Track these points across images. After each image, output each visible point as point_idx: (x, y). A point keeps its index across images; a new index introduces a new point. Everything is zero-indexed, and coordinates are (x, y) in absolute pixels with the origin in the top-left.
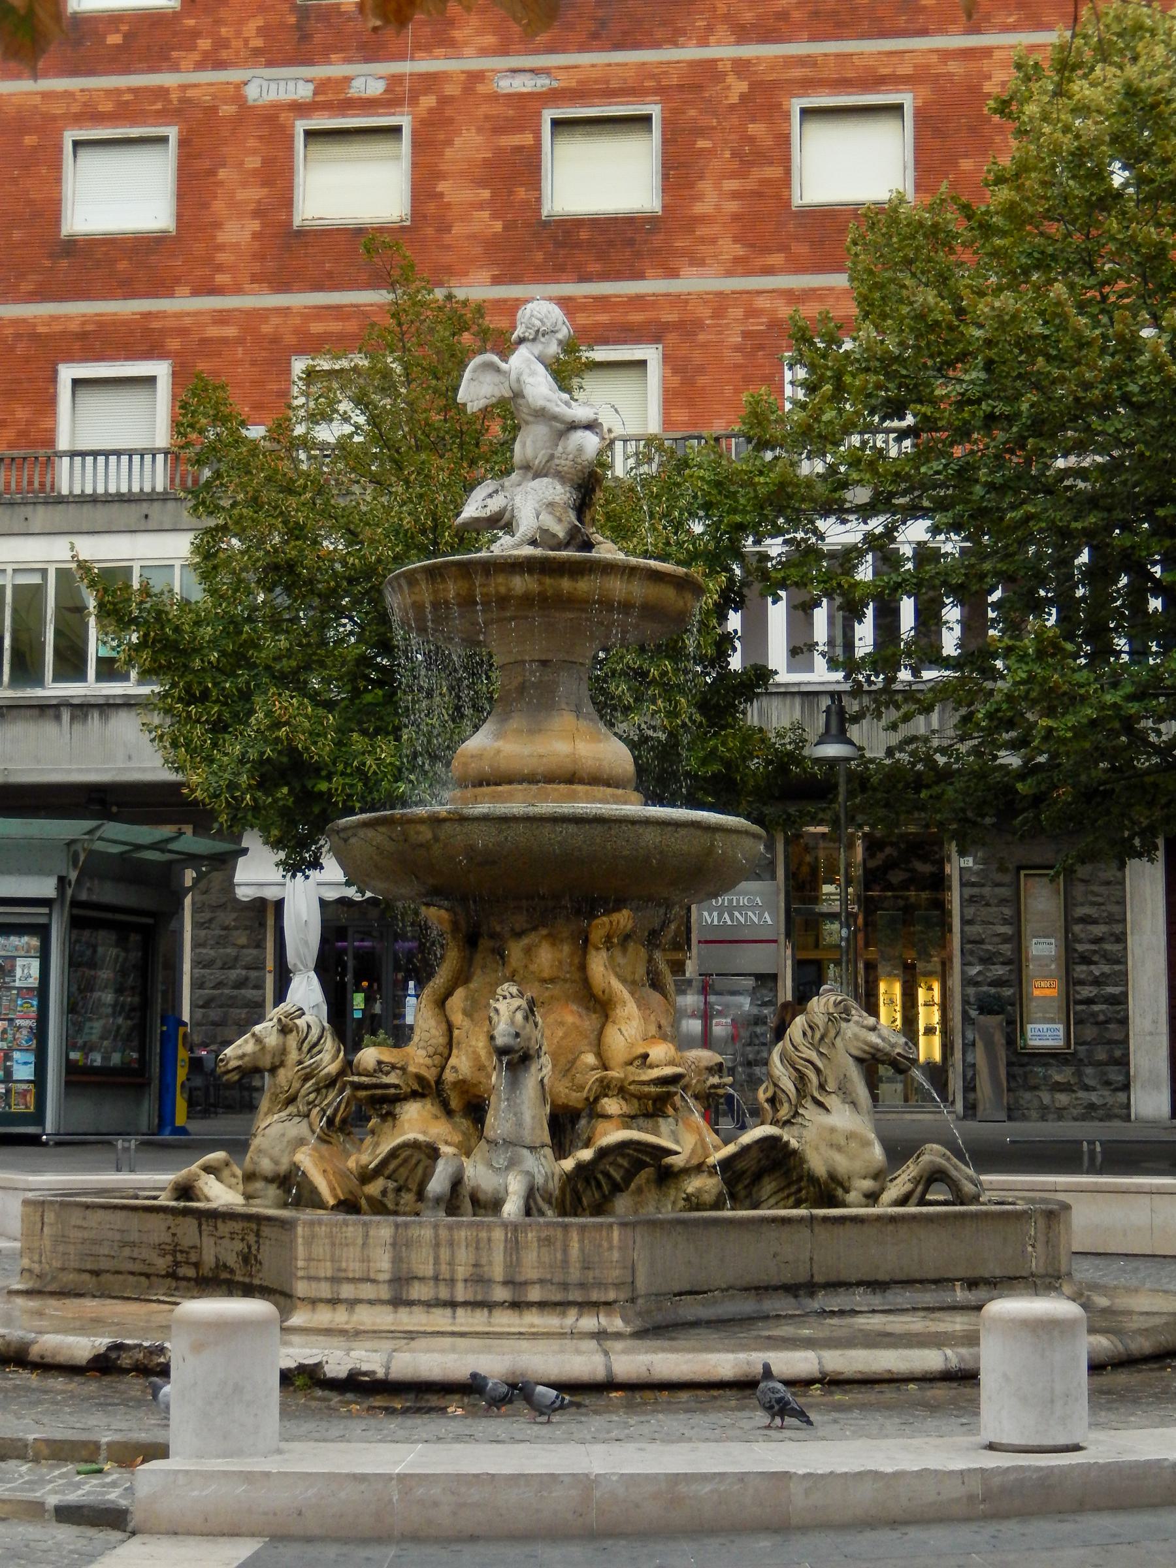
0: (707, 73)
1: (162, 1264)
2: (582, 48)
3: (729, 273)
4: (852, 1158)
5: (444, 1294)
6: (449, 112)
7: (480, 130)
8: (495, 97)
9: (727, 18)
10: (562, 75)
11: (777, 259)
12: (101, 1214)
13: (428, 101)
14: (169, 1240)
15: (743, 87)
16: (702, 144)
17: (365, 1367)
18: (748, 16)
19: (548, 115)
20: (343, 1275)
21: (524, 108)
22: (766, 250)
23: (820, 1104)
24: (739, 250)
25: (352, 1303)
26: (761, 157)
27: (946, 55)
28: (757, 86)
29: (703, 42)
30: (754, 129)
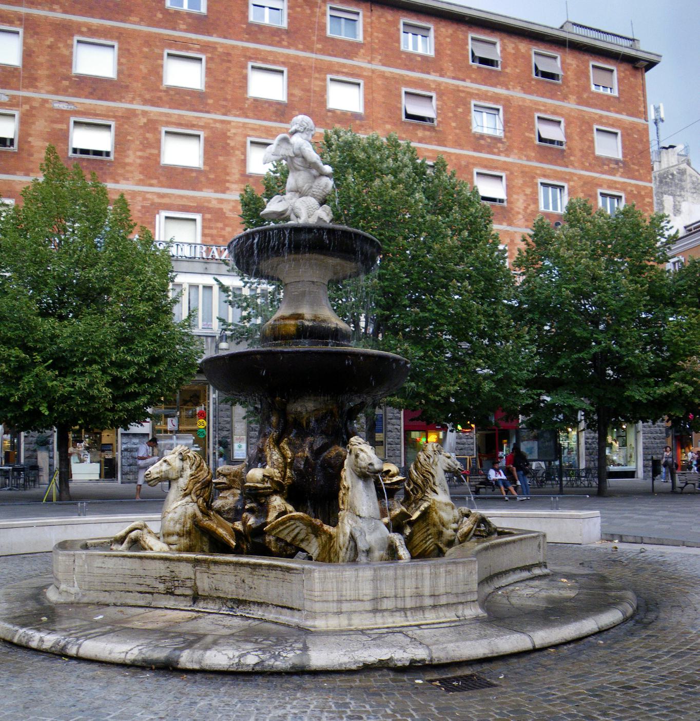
0: (132, 114)
1: (162, 587)
2: (86, 97)
3: (137, 184)
4: (449, 514)
5: (400, 605)
6: (34, 112)
7: (46, 121)
8: (52, 110)
9: (140, 96)
10: (79, 106)
11: (154, 182)
12: (114, 559)
13: (26, 107)
14: (168, 575)
15: (145, 120)
16: (129, 138)
17: (418, 657)
18: (148, 96)
19: (72, 119)
20: (344, 598)
21: (63, 116)
22: (150, 178)
23: (435, 491)
24: (141, 177)
25: (351, 613)
26: (150, 146)
27: (215, 121)
28: (150, 121)
29: (131, 102)
30: (148, 135)
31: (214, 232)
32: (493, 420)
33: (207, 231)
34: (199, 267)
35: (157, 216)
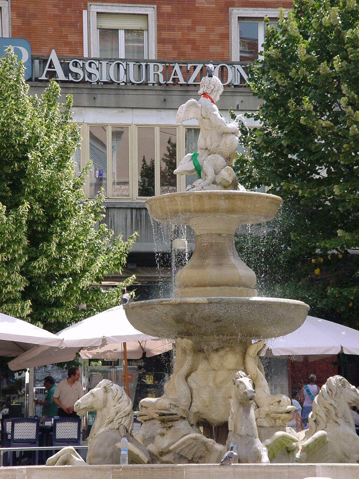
31: (177, 35)
32: (343, 333)
33: (165, 35)
34: (153, 98)
35: (85, 12)
